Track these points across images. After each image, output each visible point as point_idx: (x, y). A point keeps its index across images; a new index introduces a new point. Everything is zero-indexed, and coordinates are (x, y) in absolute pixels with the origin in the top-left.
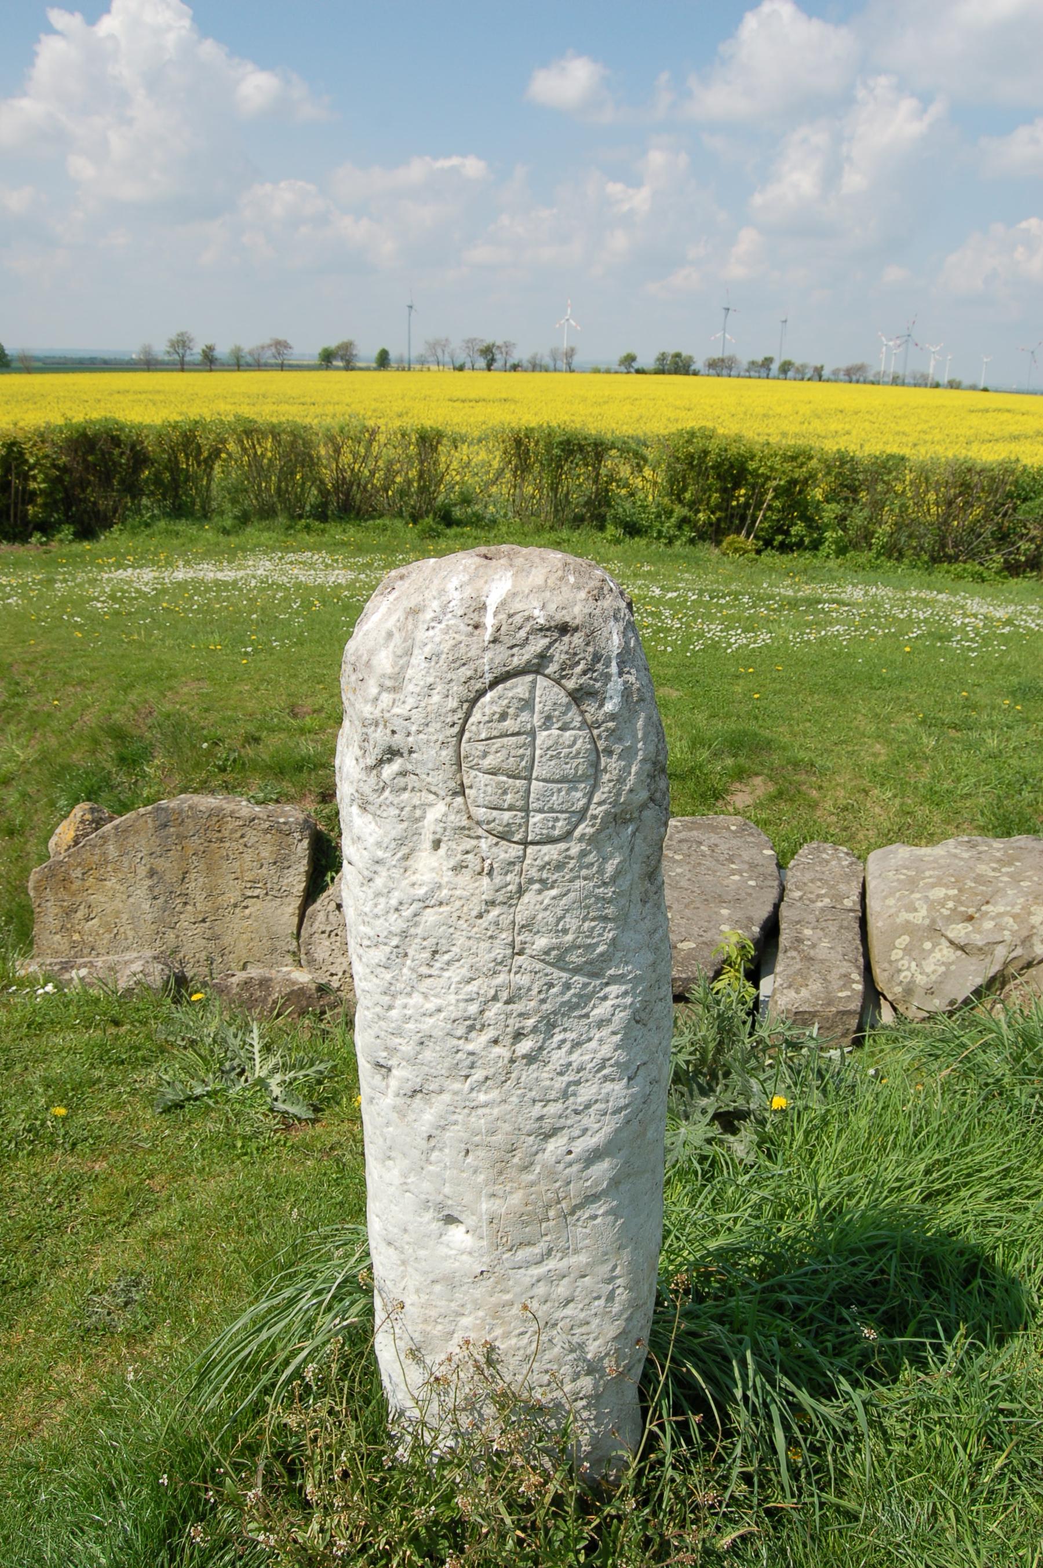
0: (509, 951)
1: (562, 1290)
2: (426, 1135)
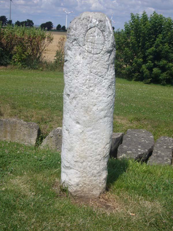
0: (90, 72)
1: (95, 137)
2: (74, 106)
